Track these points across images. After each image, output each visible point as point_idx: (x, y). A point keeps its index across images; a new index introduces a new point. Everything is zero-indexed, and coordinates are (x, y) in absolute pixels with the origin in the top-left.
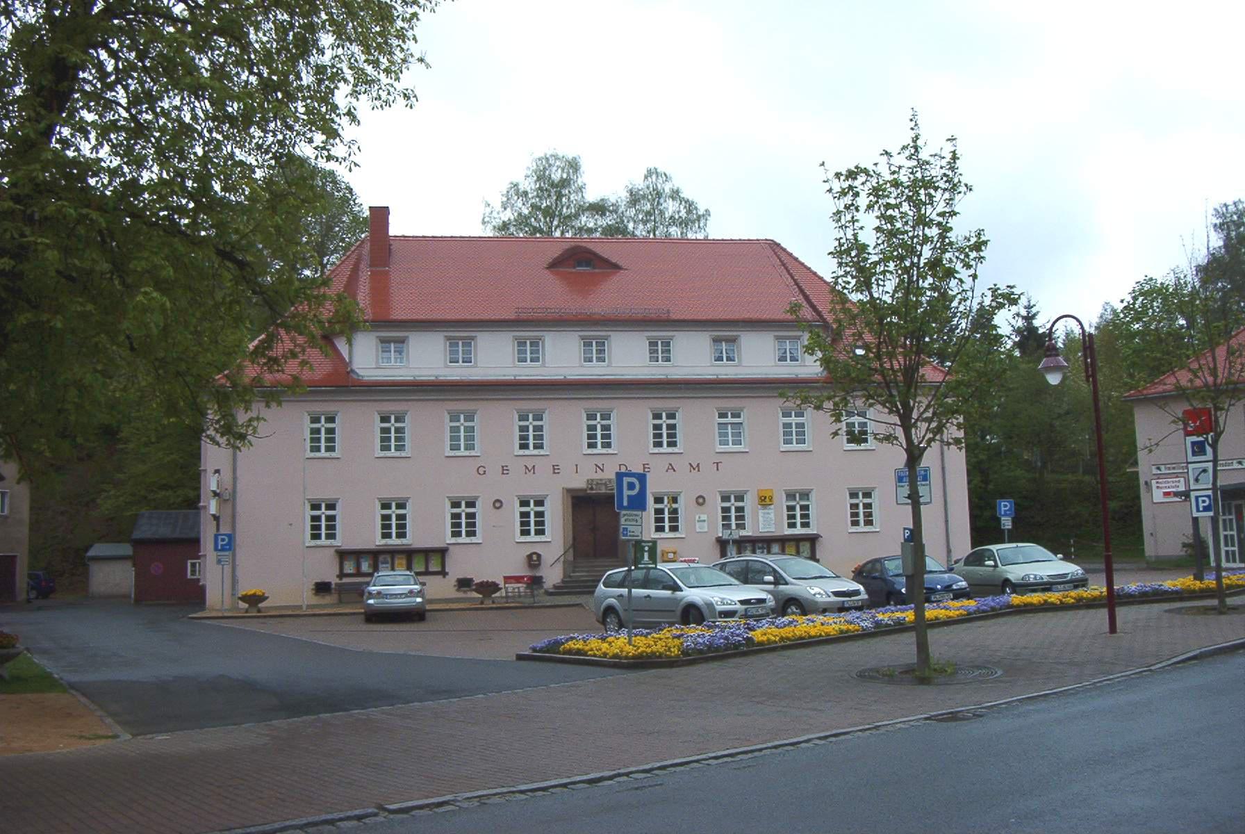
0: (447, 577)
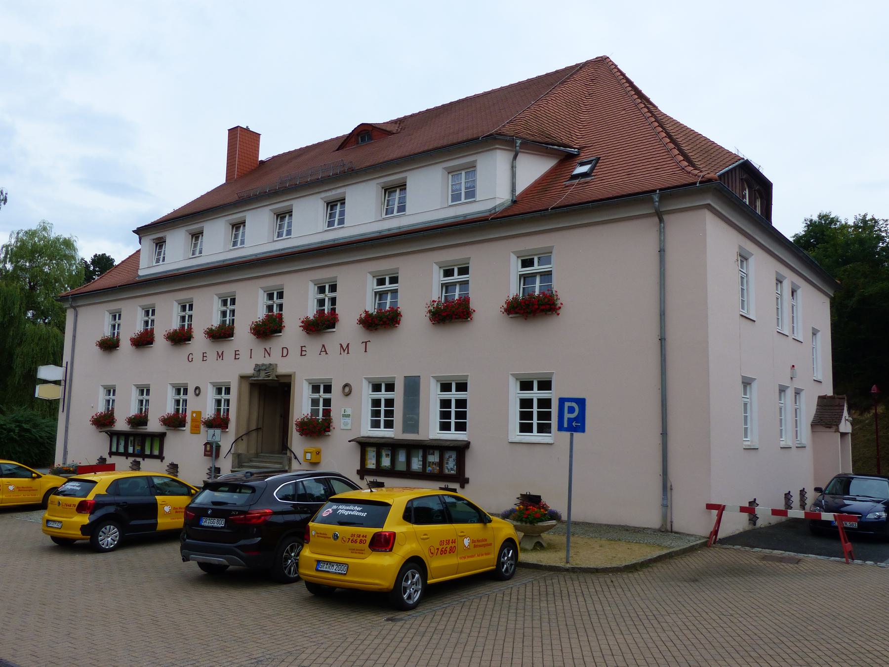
0: (467, 486)
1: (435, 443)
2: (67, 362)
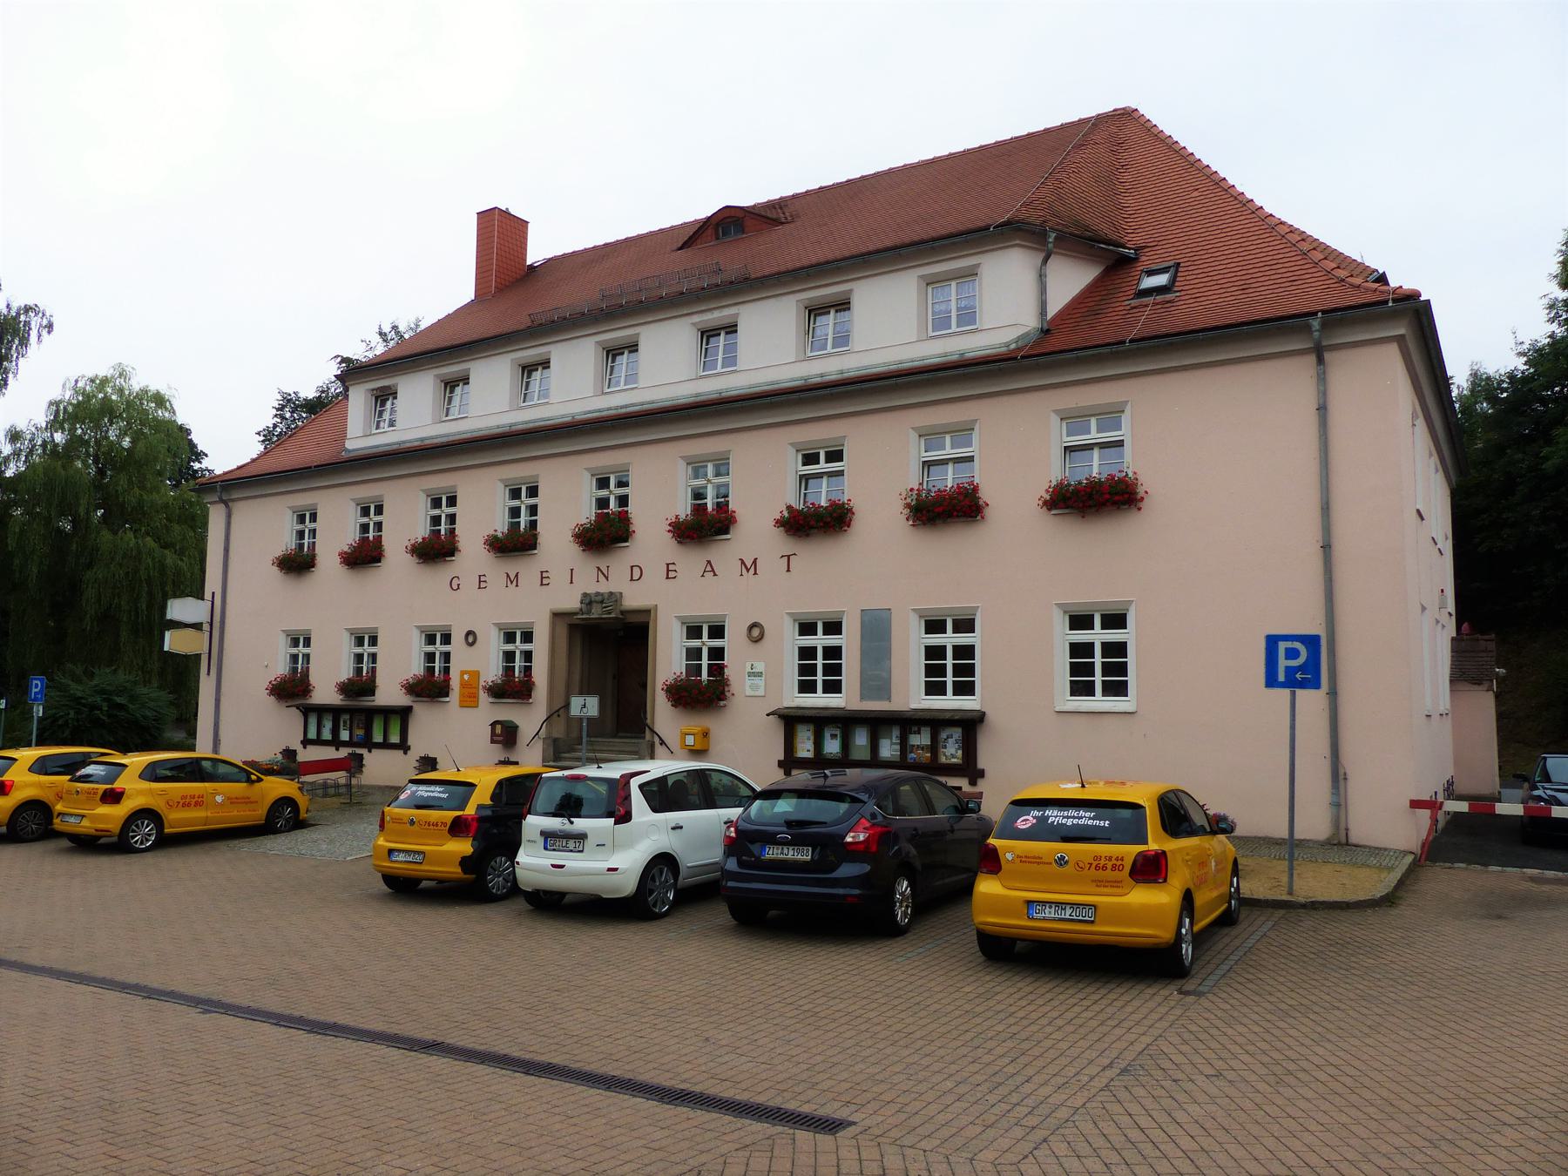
1: (927, 716)
2: (213, 593)
